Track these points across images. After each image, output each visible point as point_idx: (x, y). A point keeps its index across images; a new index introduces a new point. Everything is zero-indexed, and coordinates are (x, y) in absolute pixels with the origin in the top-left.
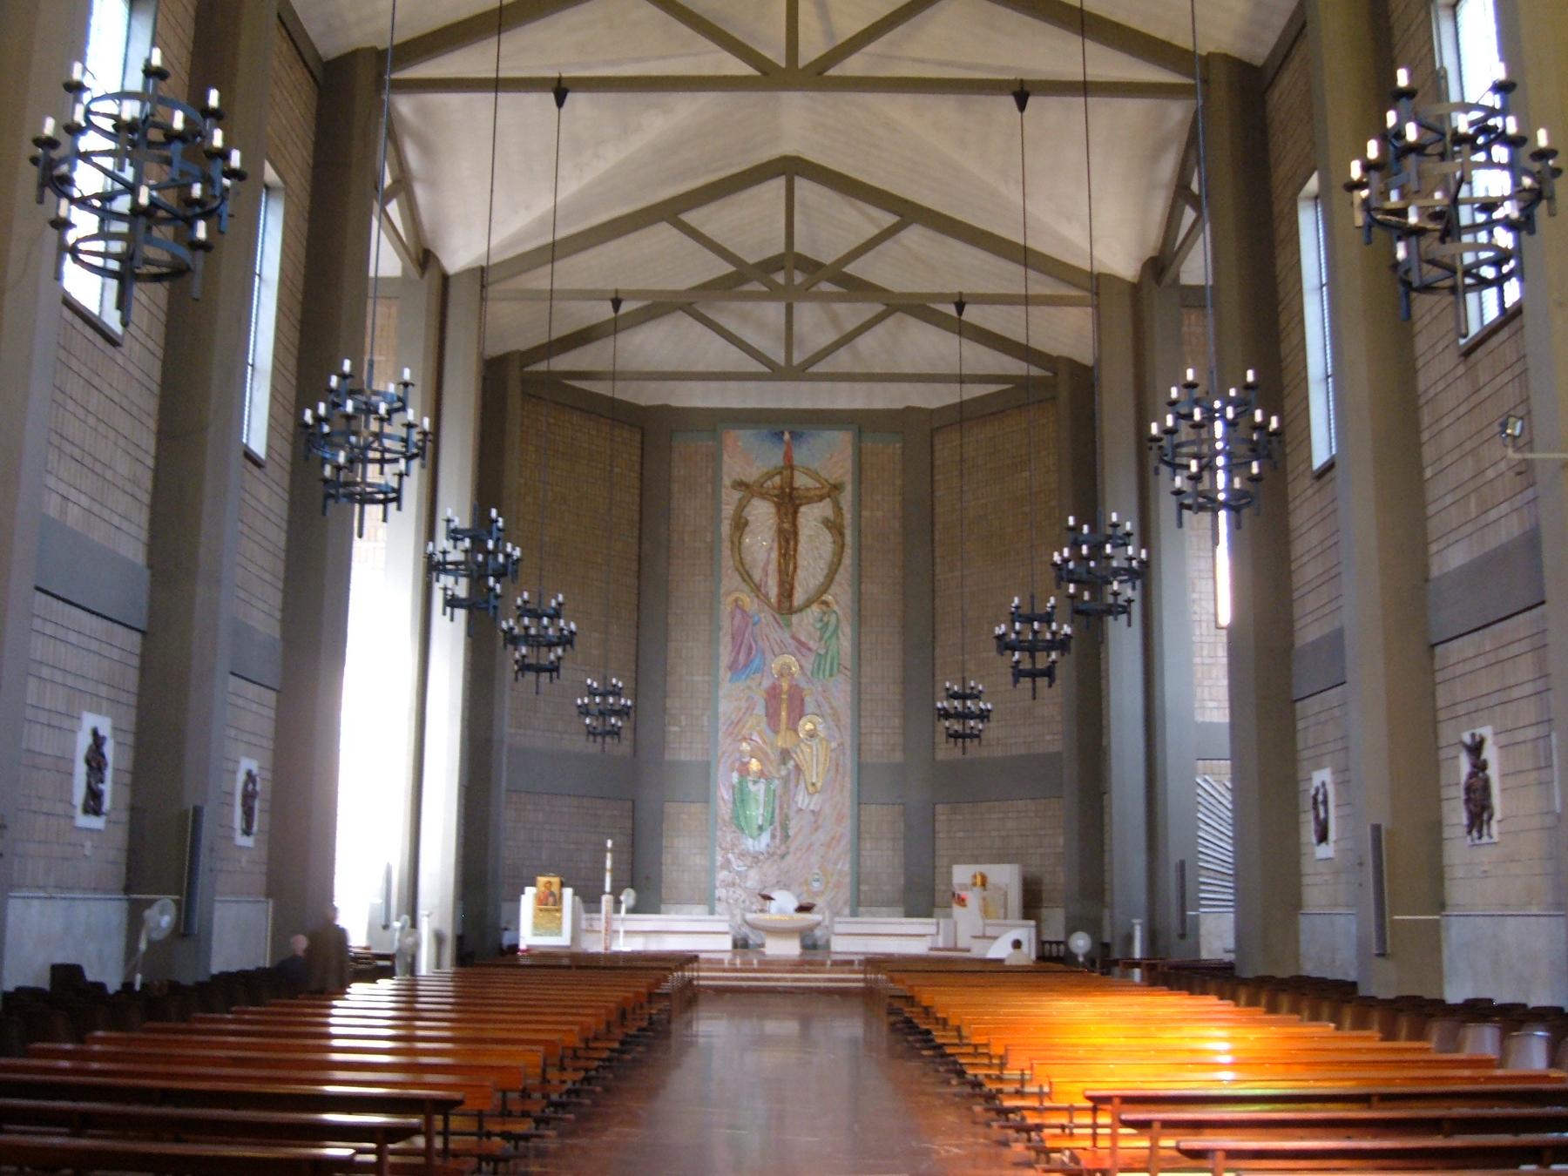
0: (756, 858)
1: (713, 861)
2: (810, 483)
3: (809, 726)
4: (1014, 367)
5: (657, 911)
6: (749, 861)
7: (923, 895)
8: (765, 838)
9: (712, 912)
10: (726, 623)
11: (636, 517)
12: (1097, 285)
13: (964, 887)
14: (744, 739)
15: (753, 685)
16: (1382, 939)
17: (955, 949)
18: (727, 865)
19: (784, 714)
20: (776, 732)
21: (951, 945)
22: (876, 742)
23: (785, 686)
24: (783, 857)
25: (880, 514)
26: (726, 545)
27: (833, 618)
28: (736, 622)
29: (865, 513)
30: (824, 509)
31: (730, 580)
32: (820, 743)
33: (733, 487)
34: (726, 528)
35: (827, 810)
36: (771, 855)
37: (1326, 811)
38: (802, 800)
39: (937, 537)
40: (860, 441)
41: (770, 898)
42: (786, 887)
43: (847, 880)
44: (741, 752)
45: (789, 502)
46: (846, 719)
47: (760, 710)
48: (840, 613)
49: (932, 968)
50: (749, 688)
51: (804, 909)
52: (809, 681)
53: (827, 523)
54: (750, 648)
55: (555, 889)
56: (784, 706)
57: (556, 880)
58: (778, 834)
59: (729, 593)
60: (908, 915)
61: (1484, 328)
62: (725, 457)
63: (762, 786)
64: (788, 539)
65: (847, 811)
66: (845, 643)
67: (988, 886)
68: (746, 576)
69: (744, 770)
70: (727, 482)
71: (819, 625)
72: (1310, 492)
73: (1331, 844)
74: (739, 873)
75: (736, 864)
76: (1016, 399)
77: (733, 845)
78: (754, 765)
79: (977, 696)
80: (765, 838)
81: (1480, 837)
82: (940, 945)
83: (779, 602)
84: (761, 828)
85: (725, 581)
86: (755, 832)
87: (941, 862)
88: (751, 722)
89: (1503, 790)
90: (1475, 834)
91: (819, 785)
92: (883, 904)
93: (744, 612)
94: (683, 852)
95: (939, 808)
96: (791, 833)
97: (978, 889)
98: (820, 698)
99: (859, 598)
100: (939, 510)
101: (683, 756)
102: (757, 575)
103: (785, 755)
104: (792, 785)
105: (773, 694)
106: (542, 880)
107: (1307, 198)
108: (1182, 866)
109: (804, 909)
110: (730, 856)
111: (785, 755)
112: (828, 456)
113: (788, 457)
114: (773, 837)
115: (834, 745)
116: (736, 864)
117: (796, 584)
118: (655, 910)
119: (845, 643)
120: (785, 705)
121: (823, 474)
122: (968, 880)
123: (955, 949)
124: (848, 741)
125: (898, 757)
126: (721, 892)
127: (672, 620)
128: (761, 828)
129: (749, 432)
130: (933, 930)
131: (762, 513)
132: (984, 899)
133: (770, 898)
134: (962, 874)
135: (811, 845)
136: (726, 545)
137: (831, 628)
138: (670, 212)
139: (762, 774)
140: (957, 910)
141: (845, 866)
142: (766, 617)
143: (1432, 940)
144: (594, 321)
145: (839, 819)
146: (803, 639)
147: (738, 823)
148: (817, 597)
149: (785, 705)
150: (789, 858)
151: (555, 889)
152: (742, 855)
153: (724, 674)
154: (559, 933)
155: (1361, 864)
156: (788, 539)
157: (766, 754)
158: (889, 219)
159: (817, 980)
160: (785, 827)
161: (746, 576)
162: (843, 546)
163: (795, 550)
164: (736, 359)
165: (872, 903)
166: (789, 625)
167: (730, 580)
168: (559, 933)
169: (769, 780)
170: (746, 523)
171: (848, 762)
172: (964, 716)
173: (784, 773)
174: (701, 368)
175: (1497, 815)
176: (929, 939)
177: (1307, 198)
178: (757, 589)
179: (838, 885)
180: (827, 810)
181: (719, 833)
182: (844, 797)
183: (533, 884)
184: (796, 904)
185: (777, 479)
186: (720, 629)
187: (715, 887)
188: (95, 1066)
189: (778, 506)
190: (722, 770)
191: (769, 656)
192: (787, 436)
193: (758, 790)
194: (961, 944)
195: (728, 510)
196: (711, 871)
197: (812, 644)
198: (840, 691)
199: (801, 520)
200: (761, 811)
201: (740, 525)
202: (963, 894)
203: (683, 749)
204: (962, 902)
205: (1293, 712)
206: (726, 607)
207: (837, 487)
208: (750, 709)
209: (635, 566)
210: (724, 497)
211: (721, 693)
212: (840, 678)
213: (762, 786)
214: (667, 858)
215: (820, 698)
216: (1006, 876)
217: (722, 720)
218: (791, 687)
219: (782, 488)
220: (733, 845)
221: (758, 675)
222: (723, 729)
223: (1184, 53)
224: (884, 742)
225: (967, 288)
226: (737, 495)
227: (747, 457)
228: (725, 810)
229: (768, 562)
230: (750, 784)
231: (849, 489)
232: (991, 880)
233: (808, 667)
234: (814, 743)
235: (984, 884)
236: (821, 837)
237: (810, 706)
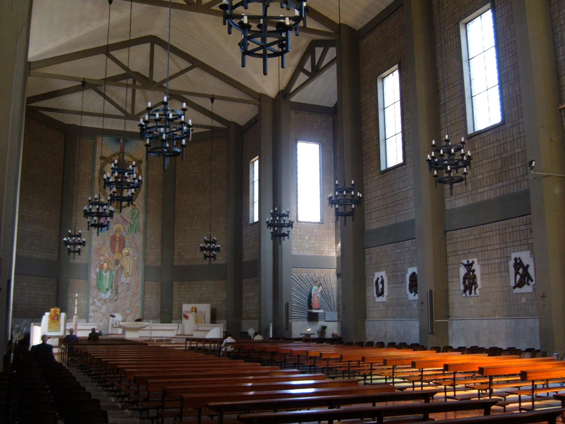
0: (105, 301)
1: (88, 302)
4: (207, 121)
6: (102, 302)
7: (167, 315)
8: (109, 293)
9: (88, 322)
12: (260, 98)
13: (188, 312)
14: (102, 255)
16: (432, 329)
17: (184, 335)
18: (94, 303)
19: (117, 246)
20: (114, 253)
23: (118, 236)
24: (116, 300)
25: (155, 173)
27: (137, 210)
29: (149, 172)
32: (131, 259)
37: (383, 286)
38: (123, 279)
41: (114, 316)
43: (140, 309)
46: (141, 249)
47: (108, 245)
49: (120, 343)
50: (104, 236)
55: (58, 313)
56: (117, 243)
57: (58, 310)
58: (114, 292)
61: (474, 133)
63: (108, 273)
69: (101, 267)
70: (98, 156)
71: (131, 213)
72: (377, 178)
73: (385, 297)
74: (98, 307)
75: (98, 304)
76: (211, 134)
77: (96, 296)
79: (215, 242)
80: (109, 293)
81: (470, 293)
82: (179, 333)
84: (107, 290)
86: (105, 291)
87: (175, 303)
88: (105, 249)
89: (482, 279)
90: (468, 292)
94: (76, 301)
95: (175, 283)
96: (119, 291)
97: (194, 313)
99: (146, 203)
103: (117, 262)
104: (120, 273)
105: (113, 238)
106: (52, 310)
107: (380, 78)
108: (287, 305)
110: (95, 300)
111: (117, 262)
114: (112, 293)
115: (136, 259)
116: (98, 304)
119: (141, 221)
120: (118, 243)
122: (190, 309)
123: (184, 335)
124: (141, 257)
125: (159, 264)
126: (91, 314)
127: (74, 208)
128: (107, 290)
129: (108, 138)
130: (176, 328)
134: (186, 307)
135: (126, 296)
137: (136, 215)
138: (107, 50)
139: (108, 269)
140: (184, 320)
141: (139, 304)
143: (445, 328)
144: (57, 89)
146: (125, 218)
147: (99, 288)
149: (118, 243)
150: (118, 301)
151: (58, 313)
152: (100, 300)
154: (59, 331)
155: (422, 303)
157: (110, 261)
158: (188, 65)
160: (117, 290)
164: (110, 109)
168: (59, 331)
169: (111, 272)
171: (141, 265)
172: (211, 250)
173: (117, 269)
174: (91, 111)
175: (479, 287)
177: (380, 78)
181: (91, 291)
182: (139, 278)
183: (49, 311)
187: (89, 312)
188: (251, 377)
190: (92, 268)
192: (121, 141)
193: (107, 275)
195: (98, 167)
197: (129, 220)
198: (139, 238)
200: (108, 283)
202: (187, 315)
204: (186, 317)
205: (365, 252)
210: (96, 162)
213: (108, 273)
216: (205, 308)
217: (93, 248)
218: (120, 236)
220: (96, 296)
223: (333, 22)
225: (216, 94)
230: (104, 273)
231: (144, 162)
232: (198, 310)
234: (128, 257)
235: (196, 311)
237: (127, 244)
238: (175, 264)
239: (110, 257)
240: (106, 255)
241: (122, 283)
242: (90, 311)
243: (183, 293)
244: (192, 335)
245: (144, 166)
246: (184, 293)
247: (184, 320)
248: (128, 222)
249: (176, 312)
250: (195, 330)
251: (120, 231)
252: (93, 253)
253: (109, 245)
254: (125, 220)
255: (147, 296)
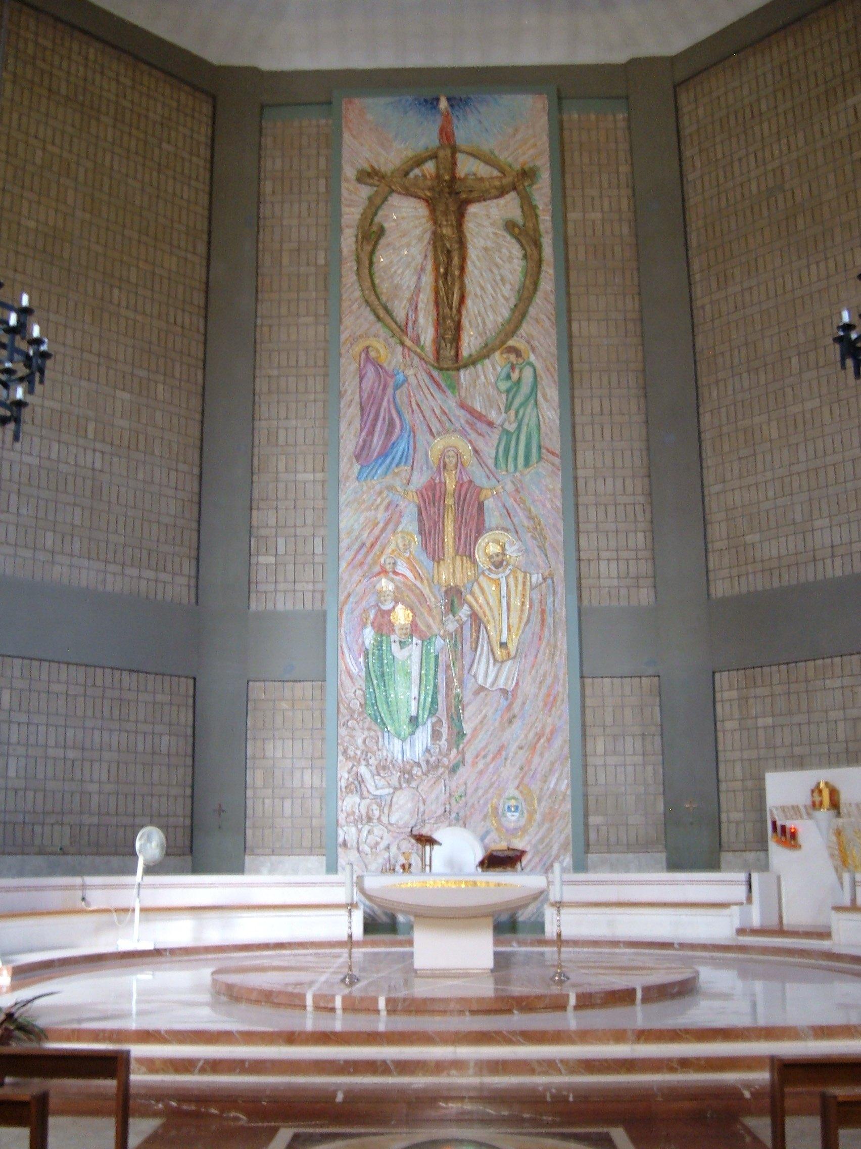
0: (407, 773)
2: (483, 170)
3: (494, 549)
5: (238, 868)
7: (700, 828)
8: (423, 736)
10: (350, 385)
11: (202, 225)
13: (795, 811)
14: (384, 571)
15: (398, 484)
17: (781, 931)
18: (357, 785)
19: (450, 528)
20: (437, 557)
21: (773, 922)
22: (607, 573)
23: (451, 485)
24: (453, 770)
26: (349, 268)
27: (528, 373)
28: (367, 384)
29: (572, 216)
30: (508, 207)
31: (356, 320)
32: (515, 581)
33: (359, 180)
34: (348, 241)
35: (528, 687)
36: (432, 767)
38: (484, 671)
39: (693, 240)
40: (560, 110)
41: (431, 841)
42: (462, 821)
43: (567, 806)
44: (379, 593)
45: (450, 200)
46: (556, 537)
47: (409, 523)
48: (539, 366)
50: (390, 488)
51: (495, 861)
52: (491, 475)
53: (510, 226)
54: (391, 424)
59: (355, 339)
60: (674, 865)
62: (346, 136)
63: (415, 649)
64: (449, 258)
65: (562, 689)
66: (550, 412)
67: (843, 809)
68: (381, 310)
69: (383, 625)
70: (349, 172)
71: (504, 386)
75: (375, 785)
78: (402, 616)
80: (423, 736)
82: (756, 920)
83: (438, 351)
84: (414, 721)
85: (348, 321)
86: (405, 728)
87: (732, 772)
88: (396, 541)
91: (512, 647)
92: (629, 848)
93: (378, 366)
94: (282, 767)
95: (722, 679)
96: (467, 728)
97: (824, 814)
98: (510, 502)
99: (568, 343)
100: (693, 199)
101: (283, 604)
102: (400, 311)
103: (454, 597)
105: (431, 496)
109: (495, 861)
110: (363, 770)
112: (513, 132)
113: (446, 135)
114: (436, 735)
115: (536, 578)
116: (375, 785)
117: (465, 323)
118: (231, 863)
120: (452, 514)
121: (504, 157)
122: (802, 798)
123: (781, 931)
125: (645, 596)
126: (347, 833)
127: (261, 385)
129: (382, 101)
130: (740, 893)
131: (407, 218)
132: (838, 833)
133: (431, 841)
134: (785, 789)
136: (349, 268)
137: (525, 389)
139: (413, 628)
140: (777, 853)
141: (561, 783)
142: (416, 374)
145: (550, 703)
146: (478, 407)
147: (375, 713)
148: (502, 341)
149: (452, 514)
152: (382, 768)
153: (348, 467)
156: (449, 258)
159: (549, 1066)
160: (456, 719)
161: (381, 310)
162: (540, 262)
163: (462, 269)
165: (609, 847)
166: (455, 386)
167: (356, 320)
169: (426, 639)
170: (382, 231)
171: (562, 606)
173: (452, 626)
176: (735, 909)
178: (401, 331)
179: (550, 817)
180: (528, 687)
182: (557, 663)
184: (480, 855)
185: (430, 167)
186: (340, 395)
189: (431, 203)
191: (422, 437)
192: (443, 104)
193: (409, 656)
194: (794, 916)
195: (351, 215)
196: (328, 796)
197: (493, 415)
198: (544, 488)
199: (470, 225)
201: (371, 235)
202: (790, 824)
203: (281, 592)
204: (788, 837)
206: (349, 367)
207: (528, 174)
208: (392, 522)
209: (198, 299)
210: (345, 193)
211: (343, 499)
212: (543, 469)
213: (415, 649)
214: (255, 777)
215: (510, 502)
217: (344, 545)
218: (459, 484)
219: (438, 176)
221: (405, 468)
222: (346, 557)
224: (618, 574)
226: (365, 191)
227: (380, 137)
228: (352, 692)
229: (418, 289)
230: (395, 647)
231: (545, 176)
232: (845, 797)
233: (488, 452)
234: (502, 576)
235: (835, 805)
236: (517, 733)
237: (493, 516)
238: (720, 589)
239: (418, 576)
240: (402, 568)
241: (482, 688)
242: (342, 817)
243: (761, 722)
244: (825, 934)
245: (547, 190)
246: (769, 721)
247: (777, 853)
248: (491, 424)
249: (737, 816)
250: (838, 909)
251: (460, 464)
252: (343, 564)
253: (414, 527)
254: (480, 417)
255: (599, 745)
